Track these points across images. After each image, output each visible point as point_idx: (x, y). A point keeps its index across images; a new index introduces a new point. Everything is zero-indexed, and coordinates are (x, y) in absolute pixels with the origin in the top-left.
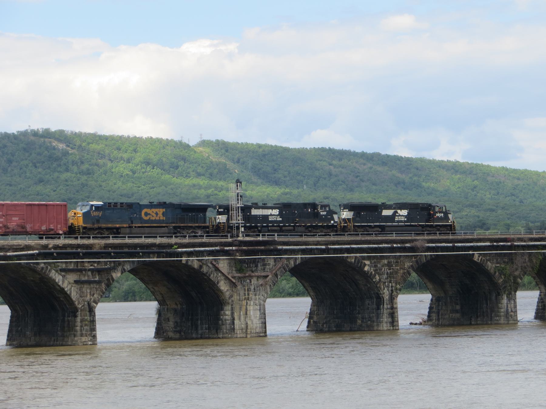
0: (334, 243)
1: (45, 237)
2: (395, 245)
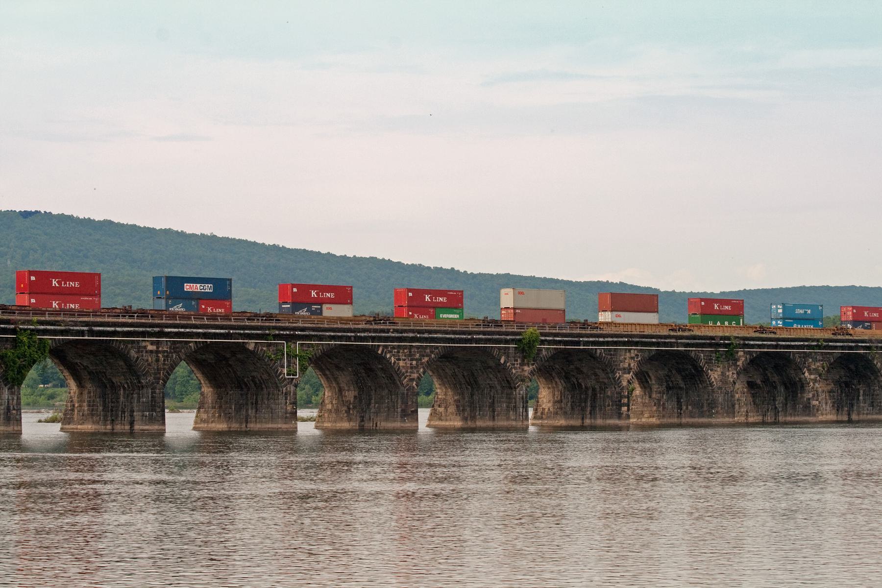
1: (92, 315)
2: (288, 332)
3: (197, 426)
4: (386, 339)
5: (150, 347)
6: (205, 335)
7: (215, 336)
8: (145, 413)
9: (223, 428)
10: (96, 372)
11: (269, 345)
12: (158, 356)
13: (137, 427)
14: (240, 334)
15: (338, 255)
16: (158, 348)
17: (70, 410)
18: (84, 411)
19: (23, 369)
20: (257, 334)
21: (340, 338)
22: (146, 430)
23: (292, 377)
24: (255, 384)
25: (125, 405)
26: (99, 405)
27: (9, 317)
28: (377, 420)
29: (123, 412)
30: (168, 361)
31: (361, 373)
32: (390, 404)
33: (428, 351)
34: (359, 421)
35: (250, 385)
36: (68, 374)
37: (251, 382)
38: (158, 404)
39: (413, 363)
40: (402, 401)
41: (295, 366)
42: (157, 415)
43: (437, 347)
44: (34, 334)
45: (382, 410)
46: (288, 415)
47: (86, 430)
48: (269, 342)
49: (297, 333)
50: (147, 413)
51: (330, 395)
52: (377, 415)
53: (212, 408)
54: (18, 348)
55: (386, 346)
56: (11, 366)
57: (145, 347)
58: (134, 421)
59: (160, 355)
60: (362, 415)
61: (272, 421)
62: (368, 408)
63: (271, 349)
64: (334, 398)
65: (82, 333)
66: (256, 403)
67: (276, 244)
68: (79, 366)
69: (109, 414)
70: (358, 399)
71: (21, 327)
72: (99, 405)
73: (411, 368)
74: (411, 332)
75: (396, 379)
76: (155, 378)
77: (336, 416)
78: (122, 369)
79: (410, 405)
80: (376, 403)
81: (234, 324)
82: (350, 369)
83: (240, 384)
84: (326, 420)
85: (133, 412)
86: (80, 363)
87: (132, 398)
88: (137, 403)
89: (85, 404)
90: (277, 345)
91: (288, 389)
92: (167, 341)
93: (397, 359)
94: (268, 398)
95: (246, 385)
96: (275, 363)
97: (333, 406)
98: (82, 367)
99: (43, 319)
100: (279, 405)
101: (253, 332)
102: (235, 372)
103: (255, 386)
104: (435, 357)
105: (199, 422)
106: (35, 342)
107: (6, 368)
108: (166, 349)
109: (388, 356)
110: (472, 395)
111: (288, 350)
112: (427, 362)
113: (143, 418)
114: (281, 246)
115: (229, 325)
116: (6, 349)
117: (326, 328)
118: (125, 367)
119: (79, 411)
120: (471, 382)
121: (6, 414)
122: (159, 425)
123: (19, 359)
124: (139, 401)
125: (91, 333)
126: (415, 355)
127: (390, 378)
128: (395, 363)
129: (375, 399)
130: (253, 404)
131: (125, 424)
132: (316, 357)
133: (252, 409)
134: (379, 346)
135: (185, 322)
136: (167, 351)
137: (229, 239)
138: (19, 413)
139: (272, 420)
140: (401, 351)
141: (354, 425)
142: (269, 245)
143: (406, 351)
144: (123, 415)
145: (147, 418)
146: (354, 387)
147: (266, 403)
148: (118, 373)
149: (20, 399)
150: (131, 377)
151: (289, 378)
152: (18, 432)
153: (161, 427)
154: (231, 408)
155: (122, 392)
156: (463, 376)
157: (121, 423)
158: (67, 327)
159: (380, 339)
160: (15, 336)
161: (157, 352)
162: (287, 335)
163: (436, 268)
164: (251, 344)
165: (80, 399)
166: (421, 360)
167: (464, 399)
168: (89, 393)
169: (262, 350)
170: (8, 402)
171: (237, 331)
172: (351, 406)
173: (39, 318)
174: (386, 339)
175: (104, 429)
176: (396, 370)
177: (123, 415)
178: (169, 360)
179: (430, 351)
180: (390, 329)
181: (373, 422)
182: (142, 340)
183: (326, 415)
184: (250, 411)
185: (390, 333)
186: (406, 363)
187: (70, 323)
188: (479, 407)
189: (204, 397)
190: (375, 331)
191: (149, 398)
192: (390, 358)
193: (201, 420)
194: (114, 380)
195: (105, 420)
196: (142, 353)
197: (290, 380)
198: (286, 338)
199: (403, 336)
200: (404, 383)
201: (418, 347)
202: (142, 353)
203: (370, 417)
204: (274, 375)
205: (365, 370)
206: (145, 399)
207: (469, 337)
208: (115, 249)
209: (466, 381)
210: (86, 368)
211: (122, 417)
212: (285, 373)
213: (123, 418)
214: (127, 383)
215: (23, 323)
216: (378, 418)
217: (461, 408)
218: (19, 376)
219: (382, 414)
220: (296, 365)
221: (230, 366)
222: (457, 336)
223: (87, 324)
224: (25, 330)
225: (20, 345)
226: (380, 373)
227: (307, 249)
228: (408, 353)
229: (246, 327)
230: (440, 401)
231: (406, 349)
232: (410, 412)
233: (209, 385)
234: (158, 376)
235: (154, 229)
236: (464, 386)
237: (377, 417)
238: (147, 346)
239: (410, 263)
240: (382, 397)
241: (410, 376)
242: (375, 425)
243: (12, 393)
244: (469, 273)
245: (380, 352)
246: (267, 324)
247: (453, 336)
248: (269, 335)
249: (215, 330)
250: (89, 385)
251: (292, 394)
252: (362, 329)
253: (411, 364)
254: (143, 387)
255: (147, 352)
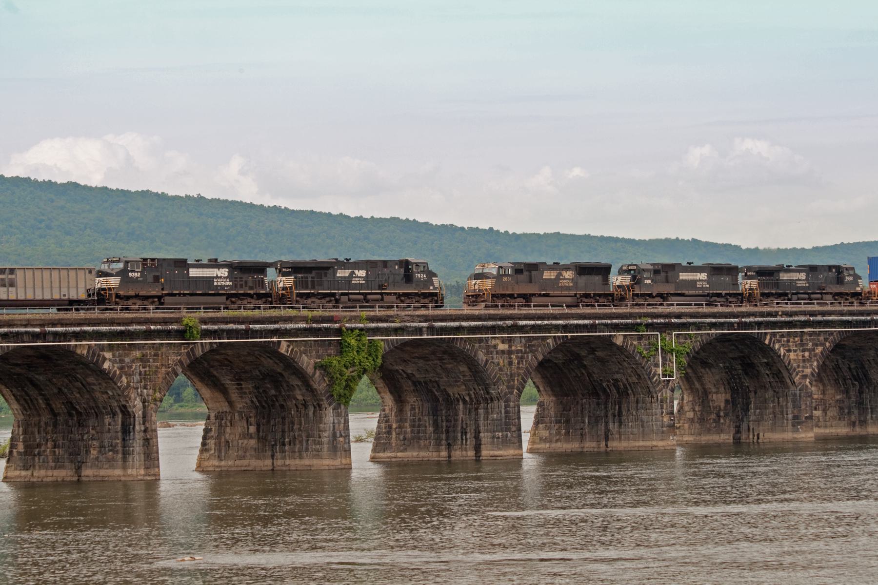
0: (749, 315)
3: (535, 446)
4: (774, 325)
5: (502, 347)
6: (565, 328)
7: (578, 328)
8: (497, 433)
9: (572, 448)
10: (425, 383)
11: (640, 338)
12: (510, 358)
13: (485, 453)
14: (606, 325)
15: (352, 216)
16: (510, 346)
17: (385, 433)
18: (405, 433)
19: (351, 381)
20: (626, 324)
21: (721, 326)
22: (499, 456)
23: (668, 378)
24: (618, 389)
25: (466, 424)
26: (427, 424)
27: (332, 314)
28: (759, 431)
29: (464, 432)
30: (523, 364)
31: (736, 370)
32: (777, 410)
33: (822, 338)
34: (734, 432)
35: (610, 390)
36: (382, 385)
37: (613, 387)
38: (513, 421)
39: (806, 355)
40: (793, 405)
41: (671, 365)
42: (512, 436)
43: (831, 333)
44: (363, 335)
45: (765, 417)
46: (665, 429)
47: (409, 459)
48: (641, 333)
49: (673, 321)
50: (500, 434)
51: (691, 399)
52: (759, 424)
53: (556, 423)
54: (344, 353)
55: (774, 334)
56: (337, 378)
57: (495, 346)
58: (480, 444)
59: (513, 356)
60: (738, 424)
61: (643, 437)
62: (746, 415)
63: (644, 342)
64: (697, 403)
65: (419, 331)
66: (620, 414)
67: (278, 205)
68: (401, 374)
69: (444, 436)
70: (731, 405)
71: (347, 325)
72: (427, 424)
73: (804, 361)
74: (802, 315)
75: (784, 375)
76: (508, 387)
77: (700, 427)
78: (464, 376)
79: (804, 409)
80: (756, 408)
81: (566, 311)
82: (721, 365)
83: (596, 392)
84: (687, 433)
85: (479, 432)
86: (402, 370)
87: (477, 414)
88: (484, 420)
89: (407, 425)
90: (649, 338)
91: (664, 395)
92: (520, 337)
93: (786, 350)
94: (637, 407)
95: (604, 390)
96: (648, 360)
97: (695, 414)
98: (405, 376)
99: (372, 314)
100: (653, 415)
101: (622, 321)
102: (590, 375)
103: (618, 392)
104: (830, 346)
105: (538, 441)
106: (364, 345)
107: (329, 381)
108: (519, 348)
109: (777, 346)
110: (861, 392)
111: (662, 344)
112: (822, 353)
113: (493, 441)
114: (283, 208)
115: (593, 314)
116: (329, 355)
117: (705, 312)
118: (468, 373)
119: (399, 434)
120: (859, 377)
121: (331, 443)
122: (515, 449)
123: (347, 369)
124: (486, 418)
125: (432, 330)
126: (807, 344)
127: (777, 376)
128: (784, 355)
129: (755, 403)
130: (614, 416)
131: (468, 449)
132: (695, 351)
133: (614, 422)
134: (766, 333)
135: (542, 312)
136: (521, 350)
137: (221, 201)
138: (347, 441)
139: (644, 436)
140: (791, 340)
141: (727, 437)
142: (269, 206)
143: (796, 339)
144: (464, 438)
145: (500, 440)
146: (725, 388)
147: (634, 413)
148: (456, 381)
149: (348, 423)
150: (476, 387)
151: (664, 381)
152: (346, 467)
153: (517, 452)
154: (584, 422)
155: (461, 406)
156: (850, 368)
157: (461, 448)
158: (403, 324)
159: (769, 325)
160: (340, 338)
161: (510, 352)
162: (661, 324)
163: (471, 229)
164: (619, 338)
165: (399, 418)
166: (814, 350)
167: (850, 398)
168: (413, 409)
169: (632, 344)
170: (334, 426)
171: (604, 321)
172: (722, 414)
173: (368, 313)
174: (774, 325)
175: (437, 457)
176: (787, 364)
177: (464, 438)
178: (524, 363)
179: (824, 339)
180: (778, 312)
181: (753, 432)
182: (491, 337)
183: (686, 426)
184: (611, 426)
185: (778, 316)
186: (797, 355)
187: (407, 318)
188: (871, 408)
189: (544, 409)
190: (762, 315)
191: (501, 413)
192: (779, 349)
193: (541, 439)
194: (450, 391)
195: (438, 444)
196: (492, 354)
197: (666, 383)
198: (660, 328)
199: (794, 320)
200: (795, 381)
201: (811, 334)
202: (492, 354)
203: (749, 427)
204: (646, 377)
205: (742, 366)
206: (495, 416)
207: (869, 318)
208: (84, 218)
209: (853, 375)
210: (409, 377)
211: (462, 439)
212: (659, 375)
213: (464, 442)
214: (469, 395)
215: (350, 320)
216: (761, 428)
217: (846, 411)
218: (346, 392)
219: (766, 423)
220: (673, 363)
221: (585, 367)
222: (855, 318)
223: (426, 319)
224: (352, 330)
225: (347, 349)
226: (764, 371)
227: (314, 210)
228: (799, 342)
229: (613, 315)
230: (816, 401)
231: (797, 337)
232: (804, 419)
233: (550, 393)
234: (512, 383)
235: (129, 192)
236: (849, 382)
237: (758, 427)
238: (498, 345)
239: (439, 224)
240: (765, 401)
241: (803, 371)
242: (756, 437)
243: (339, 415)
244: (511, 233)
245: (767, 342)
246: (637, 311)
247: (850, 318)
248: (640, 324)
249: (577, 321)
250: (412, 399)
251: (668, 401)
252: (746, 312)
253: (803, 356)
254: (492, 400)
255: (497, 353)
